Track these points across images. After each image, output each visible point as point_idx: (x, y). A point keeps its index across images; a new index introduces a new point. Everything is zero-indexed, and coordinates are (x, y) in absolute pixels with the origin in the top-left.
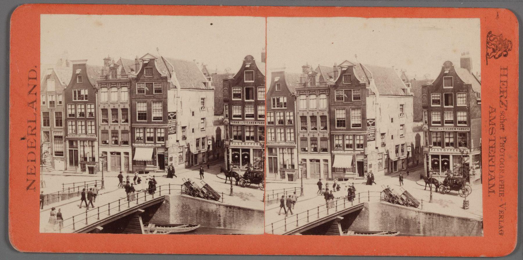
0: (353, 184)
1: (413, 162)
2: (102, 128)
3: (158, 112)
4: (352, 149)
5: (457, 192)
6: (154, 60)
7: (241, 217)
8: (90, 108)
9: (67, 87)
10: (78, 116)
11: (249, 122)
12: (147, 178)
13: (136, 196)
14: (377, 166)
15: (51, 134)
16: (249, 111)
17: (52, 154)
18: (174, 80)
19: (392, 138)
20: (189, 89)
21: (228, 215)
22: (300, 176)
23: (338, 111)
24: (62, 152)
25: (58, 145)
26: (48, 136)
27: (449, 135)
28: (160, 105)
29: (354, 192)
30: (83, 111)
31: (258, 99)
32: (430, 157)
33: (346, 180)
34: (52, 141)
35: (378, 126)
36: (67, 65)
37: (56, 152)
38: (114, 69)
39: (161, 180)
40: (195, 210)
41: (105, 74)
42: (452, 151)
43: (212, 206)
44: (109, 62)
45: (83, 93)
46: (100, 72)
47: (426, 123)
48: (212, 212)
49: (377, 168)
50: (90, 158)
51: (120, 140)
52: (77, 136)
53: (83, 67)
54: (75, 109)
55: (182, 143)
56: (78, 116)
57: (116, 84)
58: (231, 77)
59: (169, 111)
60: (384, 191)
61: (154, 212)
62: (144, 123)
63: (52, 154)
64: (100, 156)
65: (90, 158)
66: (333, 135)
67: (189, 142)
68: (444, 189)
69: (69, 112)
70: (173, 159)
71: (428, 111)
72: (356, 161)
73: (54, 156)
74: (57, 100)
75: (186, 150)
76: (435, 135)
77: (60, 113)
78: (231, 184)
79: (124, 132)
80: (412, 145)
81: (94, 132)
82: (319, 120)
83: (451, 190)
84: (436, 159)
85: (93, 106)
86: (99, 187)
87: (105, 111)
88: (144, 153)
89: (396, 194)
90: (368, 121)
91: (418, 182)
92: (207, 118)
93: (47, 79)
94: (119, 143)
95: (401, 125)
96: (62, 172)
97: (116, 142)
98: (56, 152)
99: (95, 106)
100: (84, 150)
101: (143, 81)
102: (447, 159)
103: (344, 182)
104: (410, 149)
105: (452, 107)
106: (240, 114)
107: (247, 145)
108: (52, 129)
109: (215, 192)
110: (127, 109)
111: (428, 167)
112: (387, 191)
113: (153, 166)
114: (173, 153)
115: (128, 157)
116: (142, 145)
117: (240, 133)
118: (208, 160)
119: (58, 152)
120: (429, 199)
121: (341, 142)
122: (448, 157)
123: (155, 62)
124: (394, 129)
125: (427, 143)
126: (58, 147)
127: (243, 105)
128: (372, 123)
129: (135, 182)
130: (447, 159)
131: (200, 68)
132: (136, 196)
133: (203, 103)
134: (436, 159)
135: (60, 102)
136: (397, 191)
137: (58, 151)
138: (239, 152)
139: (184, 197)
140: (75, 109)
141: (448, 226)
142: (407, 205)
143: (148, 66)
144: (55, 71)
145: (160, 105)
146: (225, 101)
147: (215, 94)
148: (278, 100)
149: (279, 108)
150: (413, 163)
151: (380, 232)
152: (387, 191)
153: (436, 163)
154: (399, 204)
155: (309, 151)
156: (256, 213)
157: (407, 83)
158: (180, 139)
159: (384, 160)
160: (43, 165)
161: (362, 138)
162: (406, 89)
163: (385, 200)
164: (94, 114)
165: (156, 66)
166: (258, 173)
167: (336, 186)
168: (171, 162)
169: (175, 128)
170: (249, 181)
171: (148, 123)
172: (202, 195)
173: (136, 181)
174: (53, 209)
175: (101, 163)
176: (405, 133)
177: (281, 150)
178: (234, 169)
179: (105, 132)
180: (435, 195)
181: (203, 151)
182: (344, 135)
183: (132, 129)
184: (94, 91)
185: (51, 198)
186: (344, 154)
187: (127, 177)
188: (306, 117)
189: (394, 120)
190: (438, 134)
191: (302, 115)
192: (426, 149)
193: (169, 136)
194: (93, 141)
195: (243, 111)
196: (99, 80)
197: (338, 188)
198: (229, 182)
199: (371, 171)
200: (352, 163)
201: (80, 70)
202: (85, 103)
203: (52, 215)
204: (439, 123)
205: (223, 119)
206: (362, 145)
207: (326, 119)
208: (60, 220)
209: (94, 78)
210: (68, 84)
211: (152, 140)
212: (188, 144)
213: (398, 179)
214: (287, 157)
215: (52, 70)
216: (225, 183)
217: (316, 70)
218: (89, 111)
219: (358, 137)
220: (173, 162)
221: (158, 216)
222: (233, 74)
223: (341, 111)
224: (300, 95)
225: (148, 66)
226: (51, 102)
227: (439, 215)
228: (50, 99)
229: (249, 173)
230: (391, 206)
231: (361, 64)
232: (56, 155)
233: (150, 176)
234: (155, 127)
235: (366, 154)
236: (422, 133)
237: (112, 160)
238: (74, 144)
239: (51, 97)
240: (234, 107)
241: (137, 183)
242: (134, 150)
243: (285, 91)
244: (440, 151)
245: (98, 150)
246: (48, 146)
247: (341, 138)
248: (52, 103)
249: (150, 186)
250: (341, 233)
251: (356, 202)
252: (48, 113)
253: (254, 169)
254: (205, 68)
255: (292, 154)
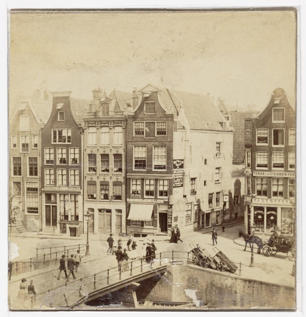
0: (153, 241)
1: (231, 215)
2: (88, 179)
3: (160, 159)
4: (153, 197)
5: (284, 254)
6: (156, 92)
7: (263, 295)
8: (73, 153)
9: (45, 126)
10: (70, 164)
11: (277, 172)
12: (144, 242)
13: (130, 265)
14: (184, 220)
15: (23, 185)
16: (278, 159)
17: (23, 211)
18: (181, 119)
19: (205, 184)
20: (201, 130)
21: (246, 291)
22: (85, 230)
23: (137, 148)
24: (37, 209)
25: (31, 199)
26: (19, 188)
27: (278, 181)
28: (144, 149)
29: (154, 252)
30: (65, 156)
31: (290, 144)
32: (252, 209)
33: (144, 235)
34: (24, 195)
35: (186, 169)
36: (46, 97)
37: (28, 208)
38: (105, 104)
39: (162, 243)
40: (204, 285)
41: (93, 110)
42: (281, 202)
43: (226, 279)
44: (100, 94)
45: (65, 133)
46: (87, 108)
47: (249, 166)
48: (227, 287)
49: (184, 222)
50: (72, 216)
51: (111, 194)
52: (56, 189)
53: (66, 100)
54: (55, 153)
55: (191, 199)
56: (58, 163)
57: (108, 123)
58: (255, 116)
59: (174, 159)
60: (192, 251)
61: (152, 287)
62: (142, 172)
63: (23, 211)
64: (85, 213)
65: (72, 216)
66: (130, 179)
67: (200, 198)
68: (269, 250)
69: (47, 157)
70: (179, 219)
71: (252, 152)
72: (158, 212)
73: (26, 213)
74: (31, 142)
75: (196, 207)
76: (259, 182)
77: (36, 159)
78: (252, 251)
79: (116, 184)
80: (230, 193)
81: (77, 183)
82: (112, 159)
83: (277, 251)
84: (259, 212)
85: (77, 151)
86: (82, 253)
87: (92, 157)
88: (142, 211)
89: (207, 256)
90: (175, 162)
91: (236, 241)
92: (223, 168)
93: (19, 115)
94: (110, 197)
95: (217, 168)
96: (36, 233)
97: (106, 197)
98: (28, 208)
99: (80, 151)
100: (64, 206)
101: (142, 119)
102: (274, 213)
103: (141, 238)
104: (227, 199)
105: (283, 146)
106: (266, 163)
107: (273, 203)
108: (25, 179)
109: (230, 262)
110: (121, 155)
111: (249, 222)
112: (196, 251)
113: (152, 227)
114: (179, 211)
115: (121, 216)
116: (140, 200)
117: (265, 187)
118: (224, 221)
119: (31, 208)
120: (250, 263)
121: (139, 188)
122: (275, 209)
123: (158, 95)
124: (209, 173)
125: (249, 191)
126: (32, 202)
127: (270, 151)
128: (180, 164)
129: (129, 248)
130: (274, 213)
131: (216, 104)
132: (130, 265)
133: (219, 148)
134: (259, 212)
135: (36, 145)
136: (209, 252)
137: (31, 206)
138: (264, 211)
139: (191, 268)
140: (55, 153)
141: (272, 297)
142: (221, 269)
143: (149, 102)
144: (30, 105)
145: (164, 149)
146: (247, 146)
147: (234, 137)
148: (60, 133)
149: (61, 143)
150: (231, 217)
151: (185, 303)
152: (196, 251)
153: (260, 217)
154: (211, 268)
155: (98, 199)
156: (282, 290)
157: (227, 116)
158: (188, 194)
159: (193, 212)
160: (13, 225)
161: (166, 183)
162: (225, 123)
163: (193, 262)
164: (78, 160)
165: (159, 100)
166: (286, 238)
167: (132, 243)
168: (176, 223)
169: (182, 180)
170: (275, 248)
171: (148, 172)
172: (214, 266)
173: (131, 246)
174: (23, 281)
175: (85, 222)
176: (221, 178)
177: (62, 197)
178: (256, 232)
179: (92, 183)
180: (257, 257)
181: (217, 209)
182: (143, 180)
183: (127, 181)
184: (79, 130)
185: (21, 266)
186: (142, 203)
187: (119, 241)
188: (95, 155)
189: (207, 162)
190: (264, 180)
191: (90, 153)
192: (248, 199)
193: (174, 189)
194: (76, 194)
195: (270, 159)
196: (87, 117)
197: (134, 246)
198: (249, 249)
199: (177, 225)
200: (153, 215)
201: (62, 104)
202: (67, 147)
203: (22, 288)
204: (265, 166)
205: (244, 169)
206: (166, 192)
207: (121, 158)
208: (32, 295)
209: (79, 115)
210: (46, 121)
211: (152, 195)
212: (199, 200)
213: (211, 236)
214: (70, 206)
215: (26, 104)
216: (245, 250)
217: (110, 96)
218: (72, 156)
219: (161, 182)
220: (178, 223)
221: (157, 291)
222: (258, 112)
223: (140, 148)
224: (89, 127)
225: (149, 102)
226: (23, 145)
227: (261, 283)
228: (22, 141)
229: (276, 238)
230: (200, 270)
231: (167, 89)
232: (29, 212)
233: (148, 240)
234: (156, 178)
235: (171, 203)
236: (243, 178)
237: (100, 220)
238: (53, 198)
239: (24, 137)
240: (259, 154)
241: (131, 248)
242: (128, 207)
243: (71, 123)
244: (265, 202)
245: (83, 206)
246: (19, 201)
247: (139, 182)
248: (25, 146)
249: (147, 253)
250: (136, 303)
251: (156, 264)
252: (19, 159)
253: (282, 233)
254: (222, 102)
255: (75, 202)
